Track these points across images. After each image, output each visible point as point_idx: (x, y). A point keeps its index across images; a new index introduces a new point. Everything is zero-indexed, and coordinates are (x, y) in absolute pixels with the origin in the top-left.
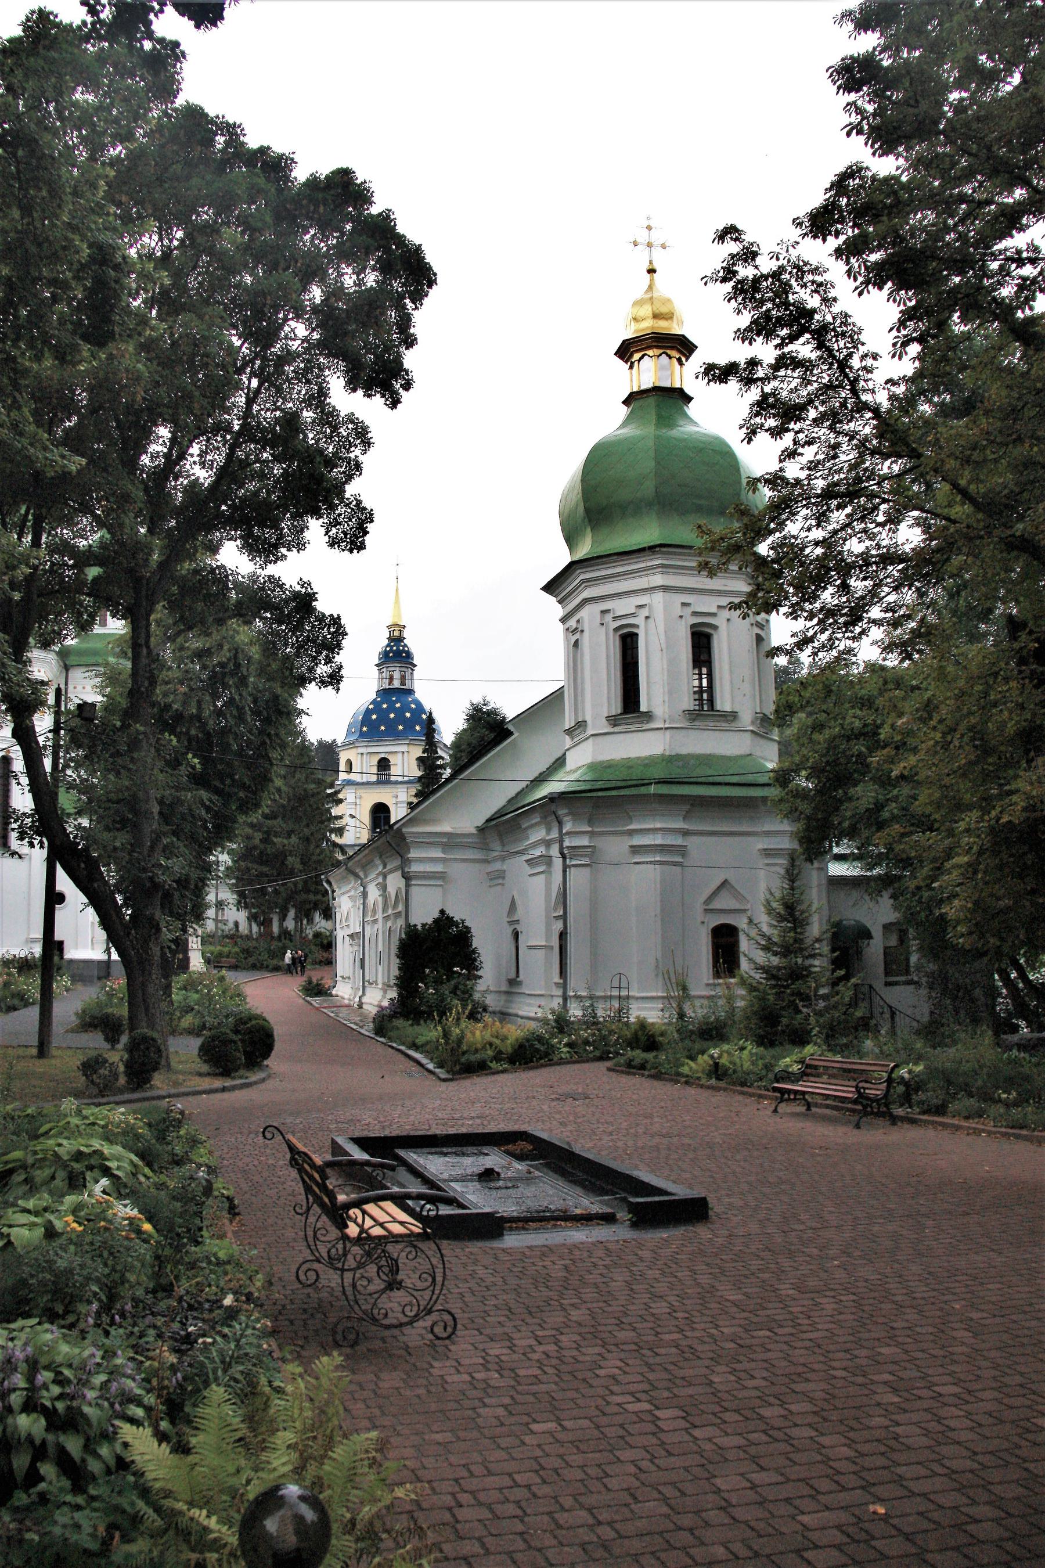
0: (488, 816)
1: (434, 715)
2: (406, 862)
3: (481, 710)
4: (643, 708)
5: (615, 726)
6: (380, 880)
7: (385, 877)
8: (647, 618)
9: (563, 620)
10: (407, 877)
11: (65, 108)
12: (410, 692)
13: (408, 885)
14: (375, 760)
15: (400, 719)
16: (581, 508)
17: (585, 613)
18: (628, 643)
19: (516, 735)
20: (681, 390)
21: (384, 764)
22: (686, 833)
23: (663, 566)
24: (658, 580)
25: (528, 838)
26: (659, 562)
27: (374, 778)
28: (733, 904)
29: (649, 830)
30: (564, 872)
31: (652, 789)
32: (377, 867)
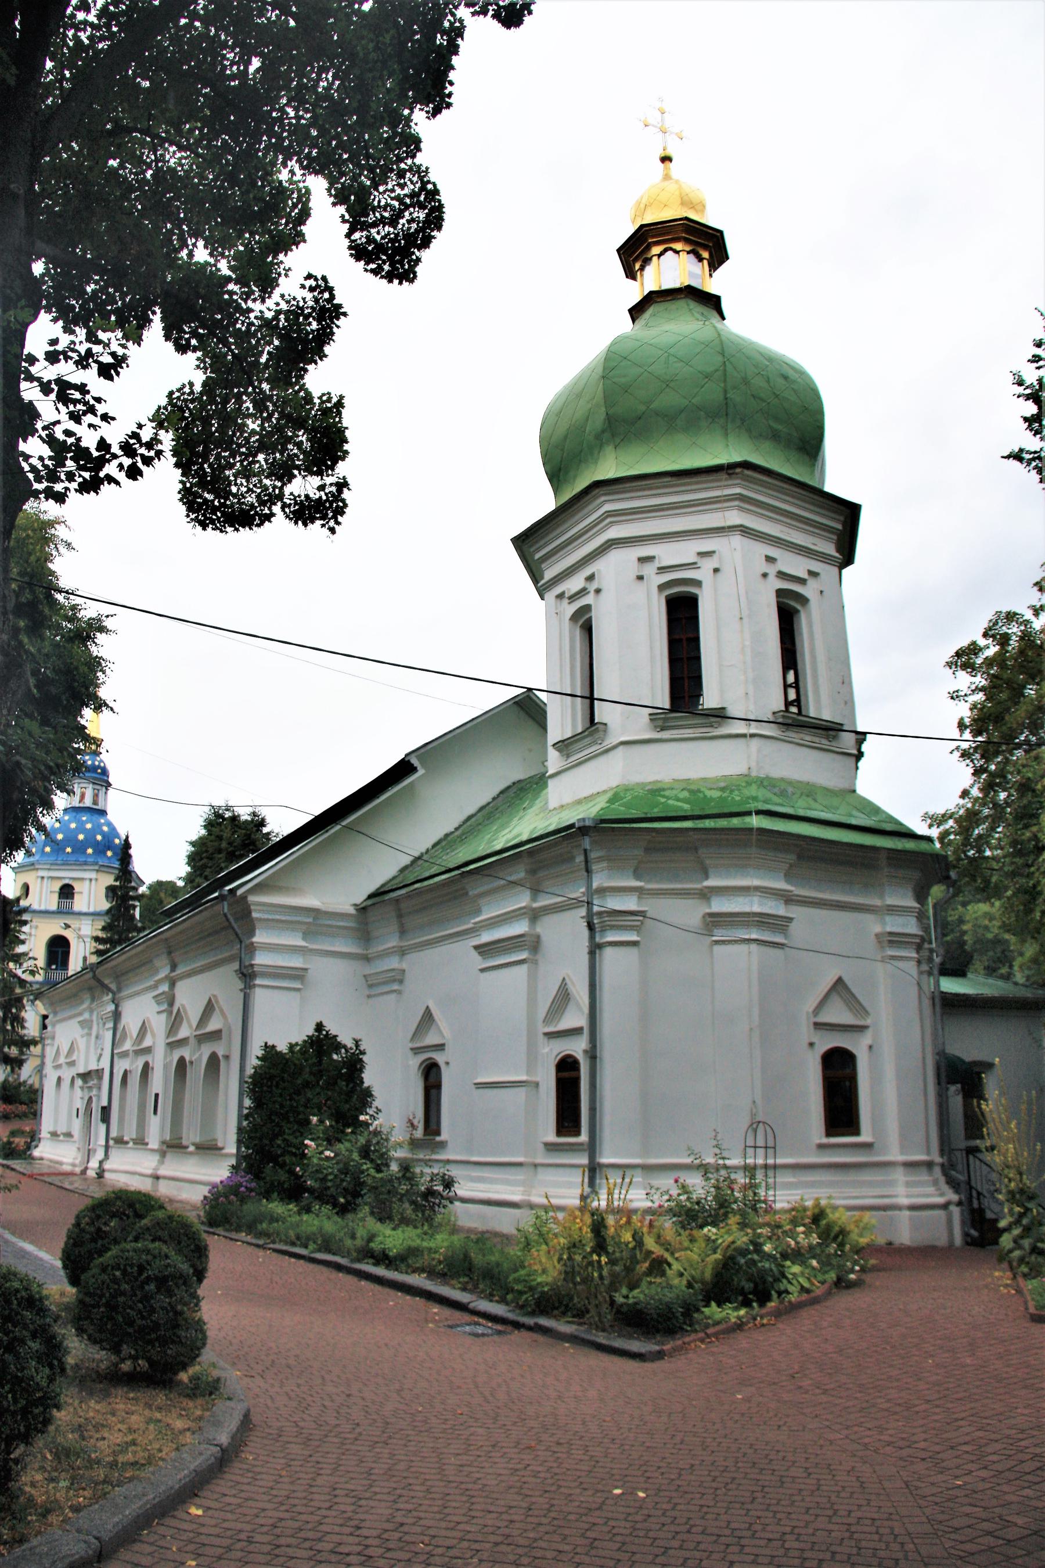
1: (131, 840)
2: (252, 949)
3: (221, 816)
4: (710, 699)
5: (663, 729)
6: (164, 988)
7: (173, 984)
8: (716, 570)
12: (103, 813)
14: (57, 886)
18: (682, 612)
19: (421, 772)
21: (67, 892)
23: (741, 498)
24: (734, 517)
25: (478, 912)
26: (738, 490)
27: (54, 907)
28: (845, 1017)
31: (755, 821)
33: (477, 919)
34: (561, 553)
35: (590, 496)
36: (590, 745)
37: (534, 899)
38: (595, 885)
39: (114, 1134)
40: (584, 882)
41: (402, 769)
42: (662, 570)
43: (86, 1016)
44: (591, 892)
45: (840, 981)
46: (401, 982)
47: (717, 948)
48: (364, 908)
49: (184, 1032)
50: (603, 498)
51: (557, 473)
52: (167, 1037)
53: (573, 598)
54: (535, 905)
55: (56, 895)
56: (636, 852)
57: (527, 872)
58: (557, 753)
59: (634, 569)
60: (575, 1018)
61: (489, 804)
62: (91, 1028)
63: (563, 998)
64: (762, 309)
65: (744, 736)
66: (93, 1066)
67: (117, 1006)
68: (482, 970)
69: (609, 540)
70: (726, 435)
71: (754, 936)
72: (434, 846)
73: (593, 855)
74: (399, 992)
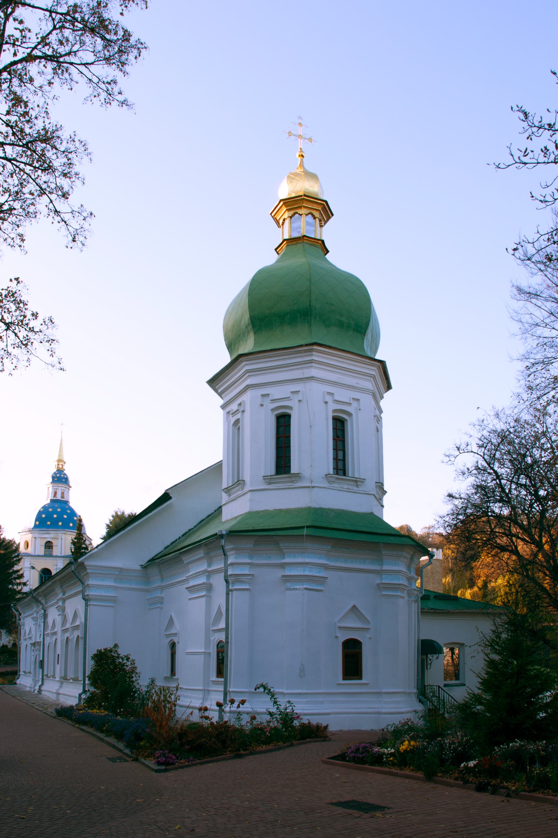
0: (150, 557)
2: (86, 587)
4: (294, 469)
5: (270, 483)
6: (60, 603)
8: (300, 401)
9: (223, 407)
10: (86, 599)
12: (67, 502)
13: (87, 605)
15: (60, 518)
16: (247, 316)
17: (246, 398)
18: (283, 422)
21: (49, 545)
22: (326, 567)
30: (227, 594)
32: (57, 595)
33: (188, 575)
34: (226, 393)
35: (238, 361)
36: (238, 490)
37: (209, 565)
39: (45, 673)
40: (223, 561)
41: (165, 497)
42: (273, 401)
43: (35, 615)
44: (226, 566)
45: (354, 606)
46: (162, 603)
47: (288, 592)
48: (145, 567)
49: (68, 626)
50: (244, 363)
51: (231, 346)
52: (62, 627)
53: (234, 413)
54: (209, 569)
55: (43, 547)
56: (248, 546)
57: (204, 553)
58: (225, 494)
59: (259, 400)
60: (222, 625)
61: (212, 513)
62: (37, 621)
64: (347, 250)
65: (309, 487)
66: (38, 640)
67: (45, 611)
68: (190, 599)
69: (247, 386)
70: (310, 326)
72: (183, 535)
73: (227, 548)
74: (161, 608)
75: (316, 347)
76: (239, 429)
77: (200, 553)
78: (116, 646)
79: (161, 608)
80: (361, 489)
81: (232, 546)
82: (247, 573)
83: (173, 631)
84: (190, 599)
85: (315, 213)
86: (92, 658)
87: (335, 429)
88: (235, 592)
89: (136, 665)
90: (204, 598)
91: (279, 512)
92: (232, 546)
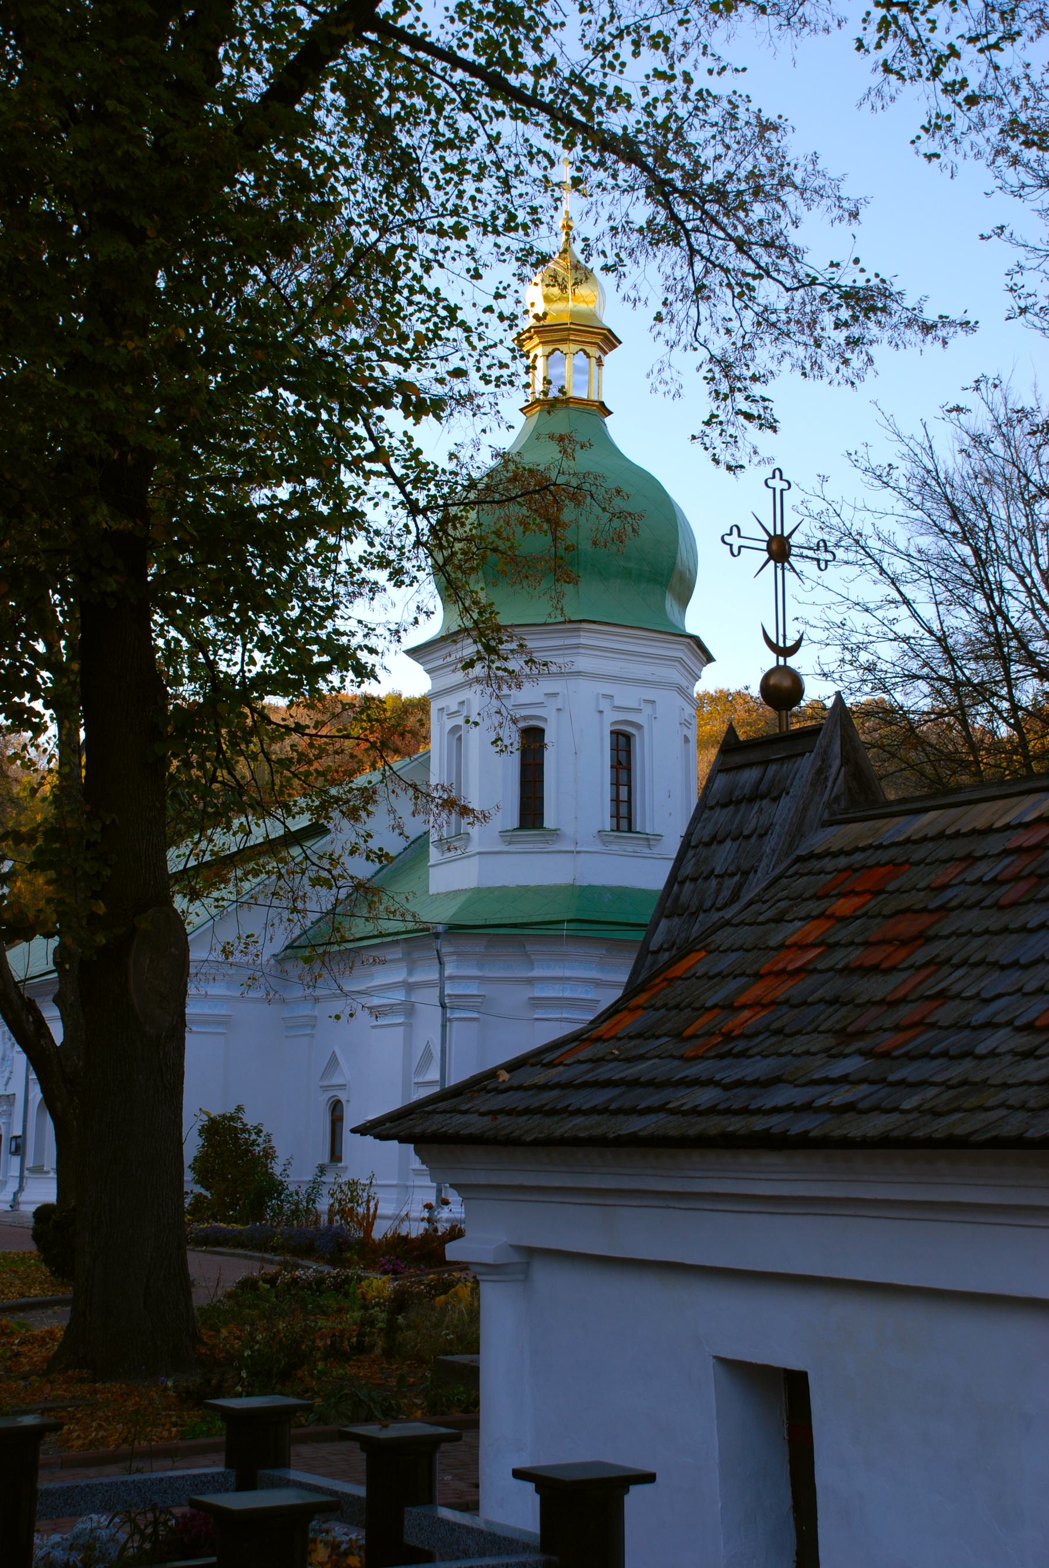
4: (549, 822)
8: (559, 710)
11: (1017, 649)
20: (602, 403)
29: (560, 979)
30: (444, 1026)
37: (410, 973)
38: (447, 973)
46: (314, 1027)
54: (411, 980)
63: (427, 1054)
68: (373, 1027)
71: (565, 1015)
73: (443, 950)
75: (585, 626)
76: (460, 738)
77: (396, 953)
78: (239, 1109)
79: (312, 1036)
80: (655, 850)
81: (451, 950)
82: (475, 992)
83: (336, 1080)
84: (373, 1027)
85: (588, 349)
86: (201, 1132)
87: (615, 748)
88: (455, 1024)
89: (273, 1144)
90: (402, 1028)
91: (525, 892)
92: (451, 950)
